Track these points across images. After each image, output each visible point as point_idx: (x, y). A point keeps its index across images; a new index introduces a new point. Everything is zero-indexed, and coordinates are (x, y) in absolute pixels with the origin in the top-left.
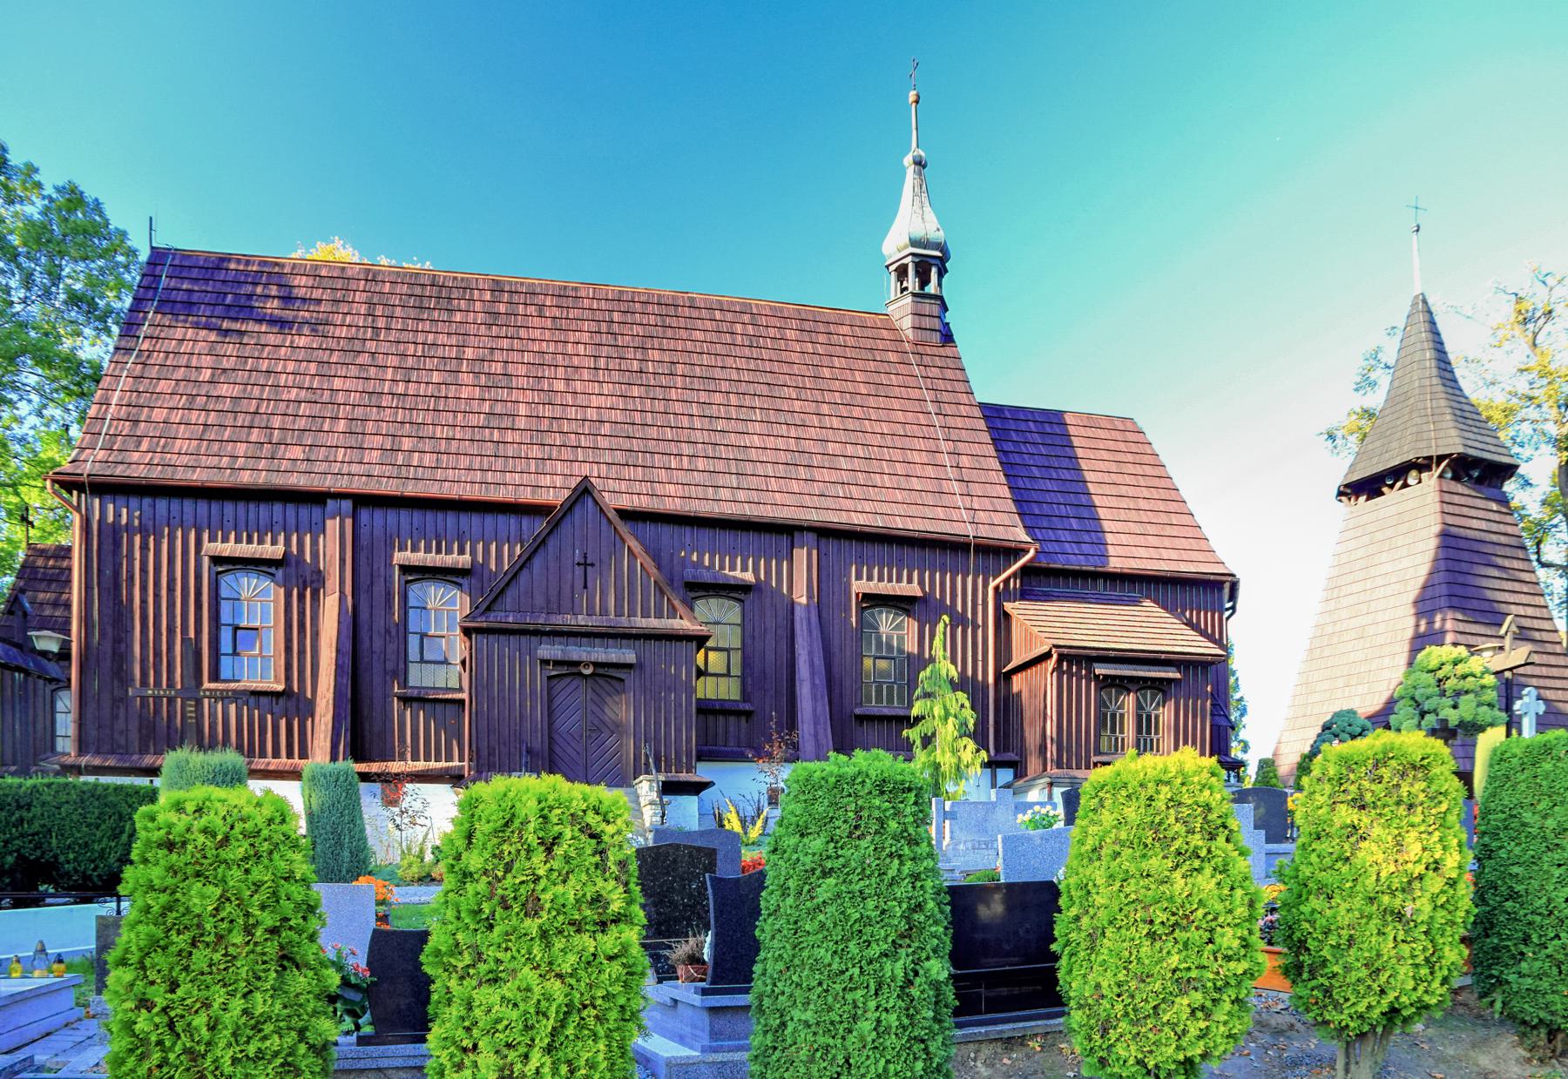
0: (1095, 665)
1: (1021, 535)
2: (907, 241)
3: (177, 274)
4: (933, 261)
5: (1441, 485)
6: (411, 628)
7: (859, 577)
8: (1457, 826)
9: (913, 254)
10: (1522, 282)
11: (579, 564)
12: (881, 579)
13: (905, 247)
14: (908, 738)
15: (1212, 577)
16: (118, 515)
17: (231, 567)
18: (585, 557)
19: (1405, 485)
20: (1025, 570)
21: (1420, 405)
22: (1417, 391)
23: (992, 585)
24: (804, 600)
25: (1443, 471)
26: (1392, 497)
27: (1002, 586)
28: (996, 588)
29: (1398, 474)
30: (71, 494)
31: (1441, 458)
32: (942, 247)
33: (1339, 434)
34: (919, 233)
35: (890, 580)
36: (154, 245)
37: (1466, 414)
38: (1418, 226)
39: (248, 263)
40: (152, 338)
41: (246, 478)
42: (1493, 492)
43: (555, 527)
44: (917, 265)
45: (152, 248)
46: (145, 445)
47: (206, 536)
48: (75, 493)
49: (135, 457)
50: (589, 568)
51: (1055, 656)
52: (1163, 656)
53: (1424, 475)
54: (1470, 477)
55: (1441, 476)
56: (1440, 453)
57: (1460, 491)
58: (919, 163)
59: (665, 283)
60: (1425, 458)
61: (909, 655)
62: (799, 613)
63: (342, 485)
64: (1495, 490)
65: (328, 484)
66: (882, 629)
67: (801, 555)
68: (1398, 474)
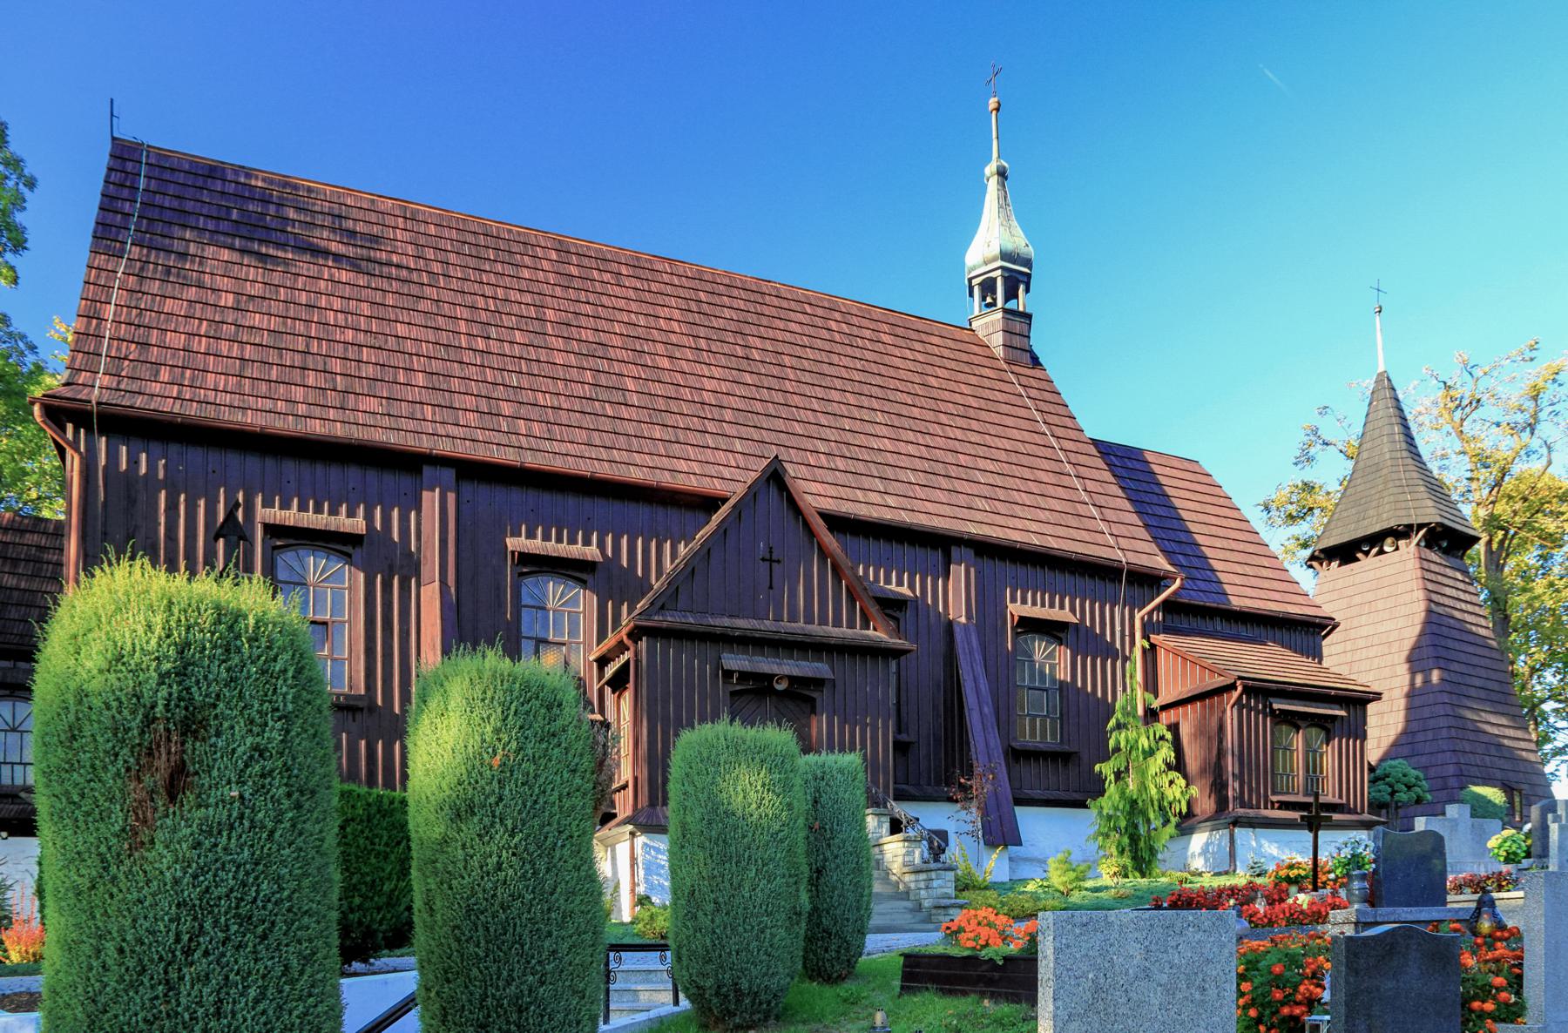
0: (1271, 700)
1: (1161, 563)
3: (156, 175)
4: (1021, 278)
5: (1419, 553)
6: (525, 631)
7: (1013, 600)
9: (1001, 267)
10: (1454, 374)
11: (763, 560)
12: (1034, 603)
13: (994, 260)
14: (1101, 772)
15: (1317, 620)
16: (133, 462)
17: (292, 541)
18: (771, 552)
19: (1381, 552)
20: (1169, 607)
21: (1395, 476)
22: (1389, 463)
23: (1138, 616)
24: (963, 620)
25: (1420, 541)
26: (1367, 565)
27: (1146, 618)
28: (1143, 618)
29: (1375, 541)
30: (64, 430)
31: (1420, 526)
32: (1028, 263)
33: (1274, 506)
34: (1009, 247)
35: (1043, 605)
36: (115, 135)
37: (1436, 489)
38: (1381, 307)
39: (248, 176)
41: (316, 428)
42: (1456, 562)
44: (1006, 279)
45: (114, 139)
46: (165, 375)
47: (259, 500)
48: (70, 427)
49: (156, 388)
51: (1240, 689)
52: (1333, 692)
53: (1402, 543)
54: (1440, 548)
55: (1418, 544)
56: (1419, 522)
57: (1434, 559)
58: (1002, 173)
59: (749, 264)
60: (1405, 526)
61: (1061, 683)
62: (959, 635)
63: (444, 447)
64: (1458, 561)
65: (425, 444)
66: (1037, 657)
68: (1375, 541)
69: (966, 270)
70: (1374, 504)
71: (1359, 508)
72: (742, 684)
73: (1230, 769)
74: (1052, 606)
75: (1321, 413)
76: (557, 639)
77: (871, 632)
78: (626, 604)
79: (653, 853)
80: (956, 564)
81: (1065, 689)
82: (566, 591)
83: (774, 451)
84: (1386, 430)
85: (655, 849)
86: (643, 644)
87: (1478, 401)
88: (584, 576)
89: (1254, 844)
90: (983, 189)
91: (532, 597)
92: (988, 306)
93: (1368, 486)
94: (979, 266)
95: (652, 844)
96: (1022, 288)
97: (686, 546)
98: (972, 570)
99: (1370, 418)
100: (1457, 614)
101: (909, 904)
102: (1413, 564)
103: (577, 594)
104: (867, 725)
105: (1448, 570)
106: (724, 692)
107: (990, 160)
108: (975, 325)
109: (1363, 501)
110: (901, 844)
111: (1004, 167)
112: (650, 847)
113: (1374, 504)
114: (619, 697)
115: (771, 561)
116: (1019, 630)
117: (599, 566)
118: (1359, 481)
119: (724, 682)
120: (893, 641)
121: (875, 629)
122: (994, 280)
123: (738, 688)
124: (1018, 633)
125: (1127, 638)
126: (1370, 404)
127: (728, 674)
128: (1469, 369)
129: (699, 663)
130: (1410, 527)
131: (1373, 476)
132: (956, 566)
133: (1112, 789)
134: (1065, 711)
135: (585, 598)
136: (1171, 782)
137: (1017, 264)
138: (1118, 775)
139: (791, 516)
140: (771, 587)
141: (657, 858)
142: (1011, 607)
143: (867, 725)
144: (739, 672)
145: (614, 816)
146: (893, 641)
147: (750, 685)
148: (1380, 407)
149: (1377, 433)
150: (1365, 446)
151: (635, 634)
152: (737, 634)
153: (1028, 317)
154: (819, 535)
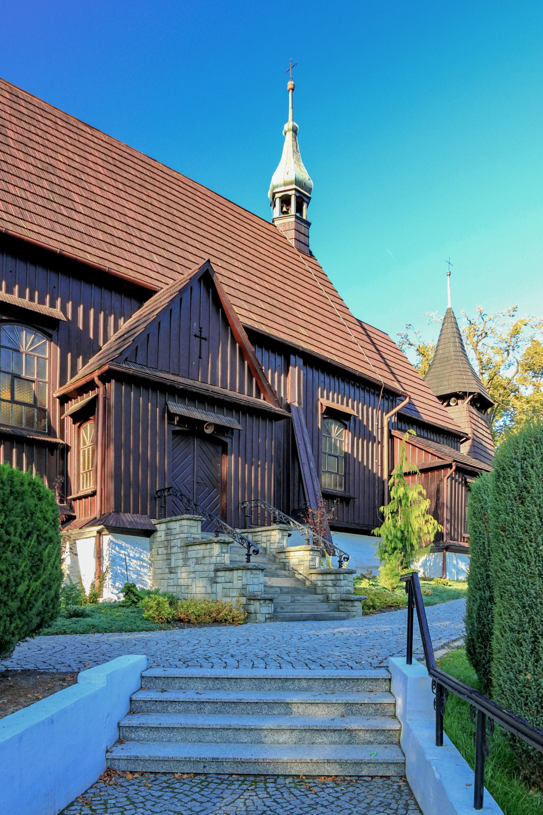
0: (466, 476)
2: (293, 179)
4: (305, 199)
8: (418, 569)
11: (196, 336)
13: (290, 183)
18: (201, 331)
19: (449, 405)
21: (457, 365)
22: (454, 357)
24: (296, 404)
31: (470, 393)
32: (309, 190)
40: (253, 803)
43: (272, 224)
44: (297, 198)
50: (203, 341)
51: (454, 468)
53: (459, 402)
54: (476, 406)
55: (468, 403)
58: (295, 131)
60: (463, 392)
61: (346, 454)
66: (333, 435)
67: (294, 371)
69: (271, 187)
70: (446, 378)
71: (439, 380)
72: (181, 427)
73: (445, 516)
74: (342, 403)
75: (407, 328)
76: (28, 377)
77: (261, 401)
78: (81, 357)
79: (117, 549)
80: (292, 366)
81: (347, 456)
82: (36, 340)
83: (207, 257)
84: (452, 340)
85: (118, 545)
86: (112, 385)
87: (486, 333)
88: (50, 331)
89: (455, 562)
90: (283, 139)
91: (9, 341)
92: (283, 213)
93: (443, 368)
94: (281, 186)
95: (117, 542)
96: (305, 205)
97: (124, 322)
98: (302, 372)
99: (444, 332)
100: (484, 443)
101: (321, 597)
102: (465, 413)
103: (45, 343)
104: (258, 466)
105: (479, 419)
106: (168, 431)
107: (287, 121)
108: (276, 223)
109: (440, 376)
110: (308, 553)
111: (297, 128)
112: (116, 544)
113: (446, 378)
114: (79, 427)
115: (201, 338)
116: (325, 416)
117: (61, 325)
118: (437, 365)
119: (169, 423)
120: (277, 409)
121: (264, 399)
122: (290, 196)
123: (178, 428)
124: (324, 418)
125: (380, 430)
126: (443, 325)
127: (172, 416)
128: (482, 315)
129: (152, 406)
130: (465, 393)
131: (445, 364)
132: (293, 368)
133: (388, 522)
134: (347, 472)
135: (50, 348)
136: (427, 521)
137: (304, 190)
138: (394, 513)
139: (212, 308)
140: (200, 357)
141: (120, 553)
142: (321, 400)
143: (258, 466)
144: (180, 416)
145: (74, 518)
146: (277, 409)
147: (186, 428)
148: (449, 327)
149: (447, 340)
150: (440, 347)
151: (105, 378)
152: (181, 387)
153: (309, 224)
154: (233, 325)
